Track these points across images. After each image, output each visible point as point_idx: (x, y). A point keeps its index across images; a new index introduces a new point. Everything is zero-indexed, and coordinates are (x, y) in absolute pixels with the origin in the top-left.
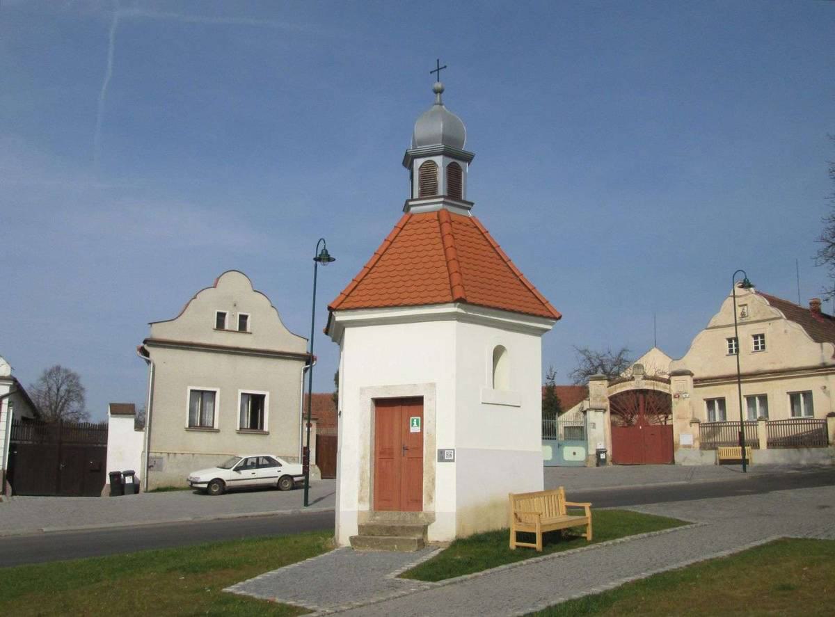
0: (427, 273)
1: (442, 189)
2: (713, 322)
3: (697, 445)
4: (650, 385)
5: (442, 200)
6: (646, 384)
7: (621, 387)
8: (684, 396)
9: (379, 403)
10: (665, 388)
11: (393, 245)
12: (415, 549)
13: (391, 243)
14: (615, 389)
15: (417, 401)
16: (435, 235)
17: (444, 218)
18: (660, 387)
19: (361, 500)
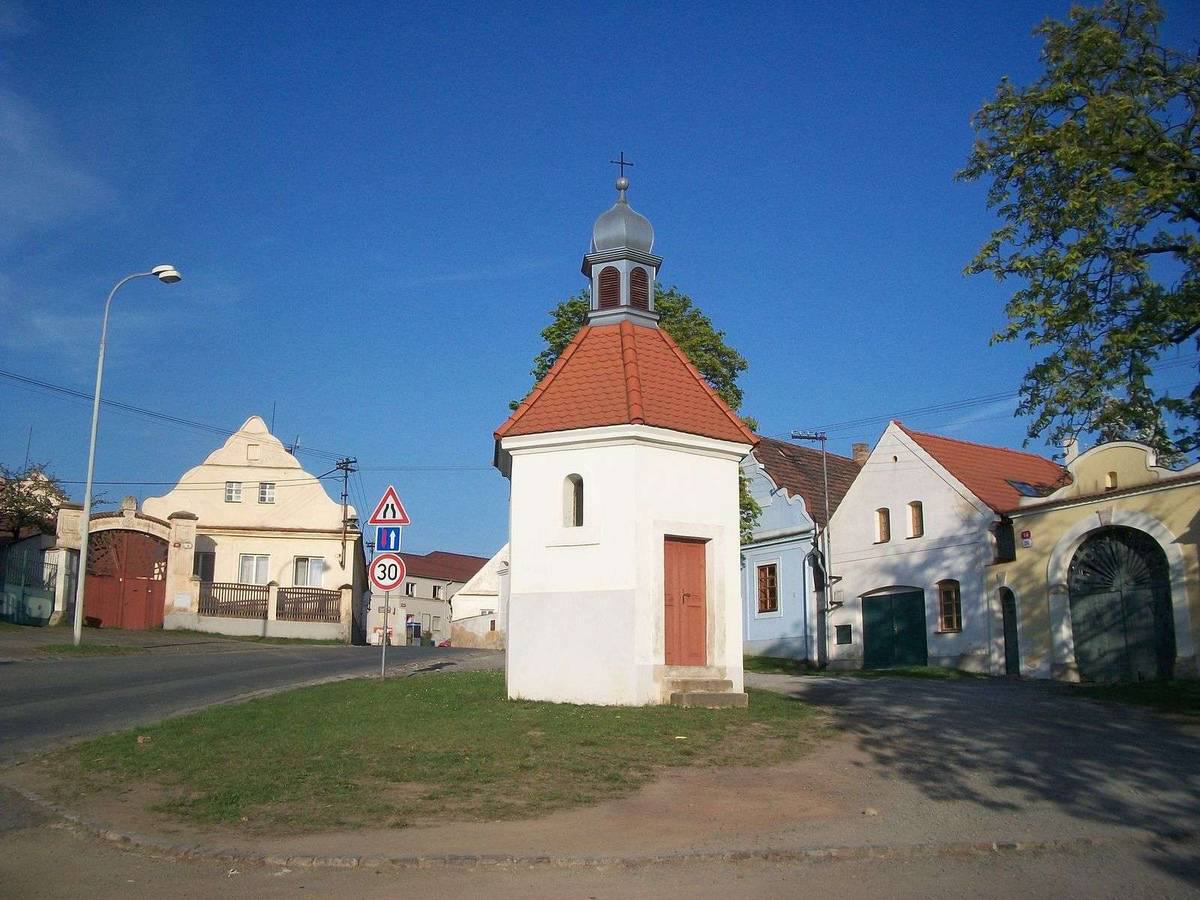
0: (594, 389)
1: (624, 296)
2: (206, 462)
3: (196, 609)
4: (145, 526)
5: (625, 310)
6: (139, 524)
7: (105, 523)
8: (186, 545)
9: (668, 538)
10: (164, 532)
11: (581, 347)
12: (833, 721)
13: (579, 345)
14: (96, 525)
15: (703, 541)
16: (613, 350)
17: (627, 330)
18: (158, 531)
19: (655, 652)
